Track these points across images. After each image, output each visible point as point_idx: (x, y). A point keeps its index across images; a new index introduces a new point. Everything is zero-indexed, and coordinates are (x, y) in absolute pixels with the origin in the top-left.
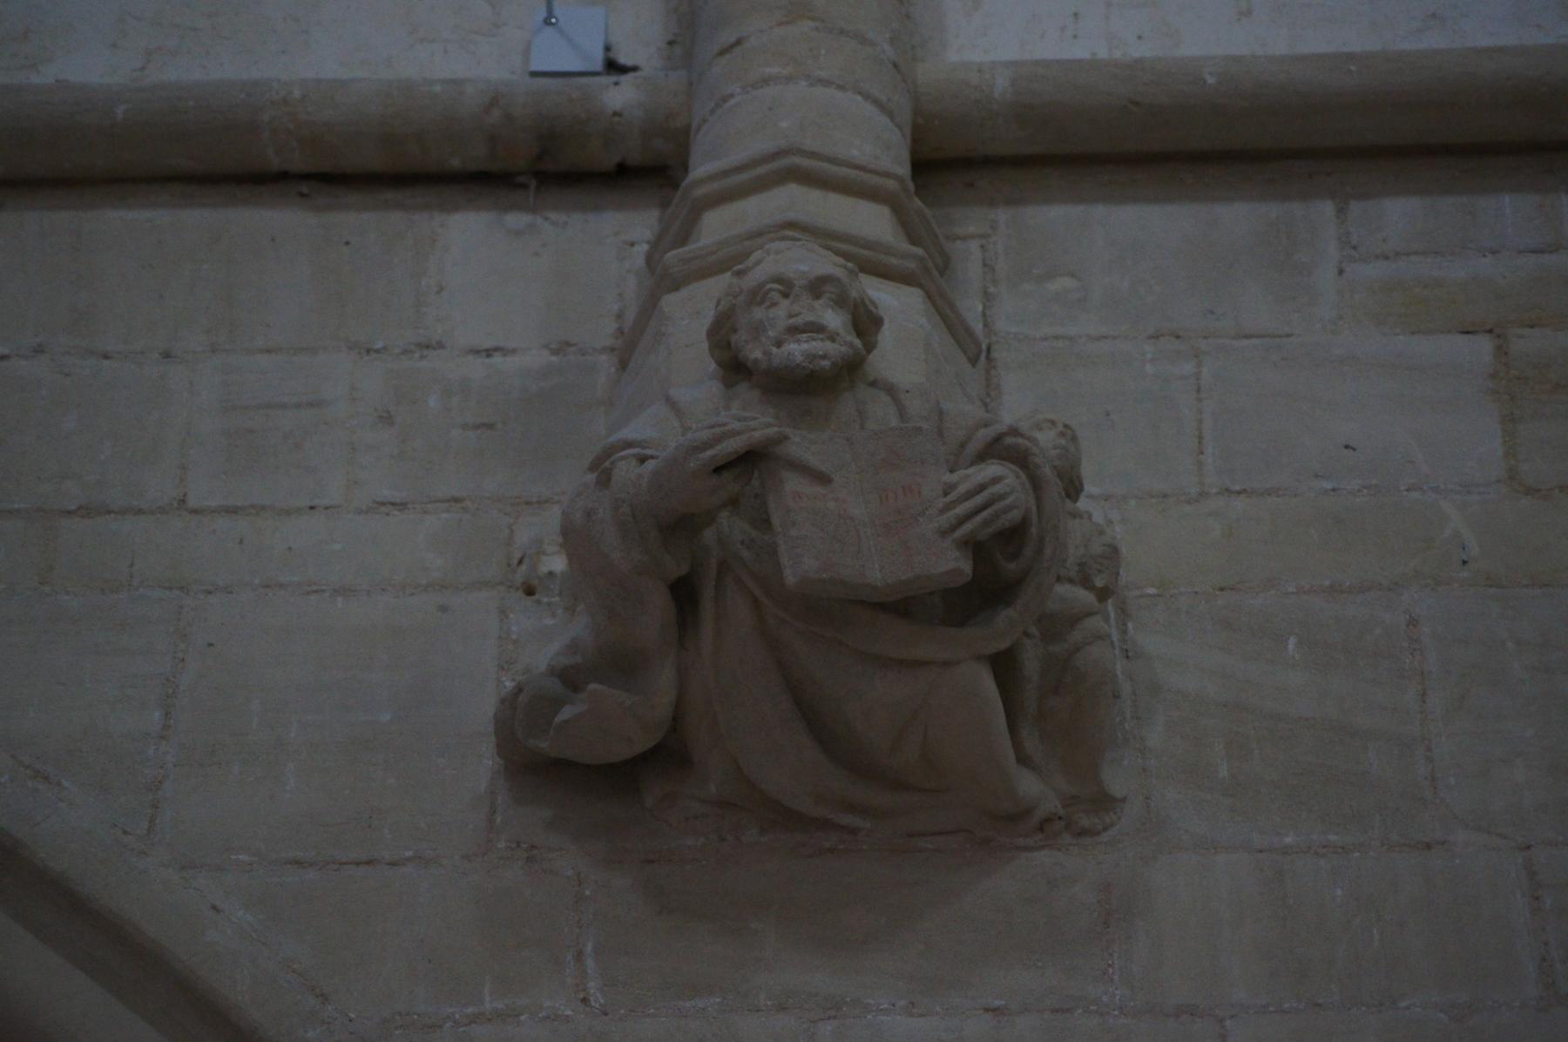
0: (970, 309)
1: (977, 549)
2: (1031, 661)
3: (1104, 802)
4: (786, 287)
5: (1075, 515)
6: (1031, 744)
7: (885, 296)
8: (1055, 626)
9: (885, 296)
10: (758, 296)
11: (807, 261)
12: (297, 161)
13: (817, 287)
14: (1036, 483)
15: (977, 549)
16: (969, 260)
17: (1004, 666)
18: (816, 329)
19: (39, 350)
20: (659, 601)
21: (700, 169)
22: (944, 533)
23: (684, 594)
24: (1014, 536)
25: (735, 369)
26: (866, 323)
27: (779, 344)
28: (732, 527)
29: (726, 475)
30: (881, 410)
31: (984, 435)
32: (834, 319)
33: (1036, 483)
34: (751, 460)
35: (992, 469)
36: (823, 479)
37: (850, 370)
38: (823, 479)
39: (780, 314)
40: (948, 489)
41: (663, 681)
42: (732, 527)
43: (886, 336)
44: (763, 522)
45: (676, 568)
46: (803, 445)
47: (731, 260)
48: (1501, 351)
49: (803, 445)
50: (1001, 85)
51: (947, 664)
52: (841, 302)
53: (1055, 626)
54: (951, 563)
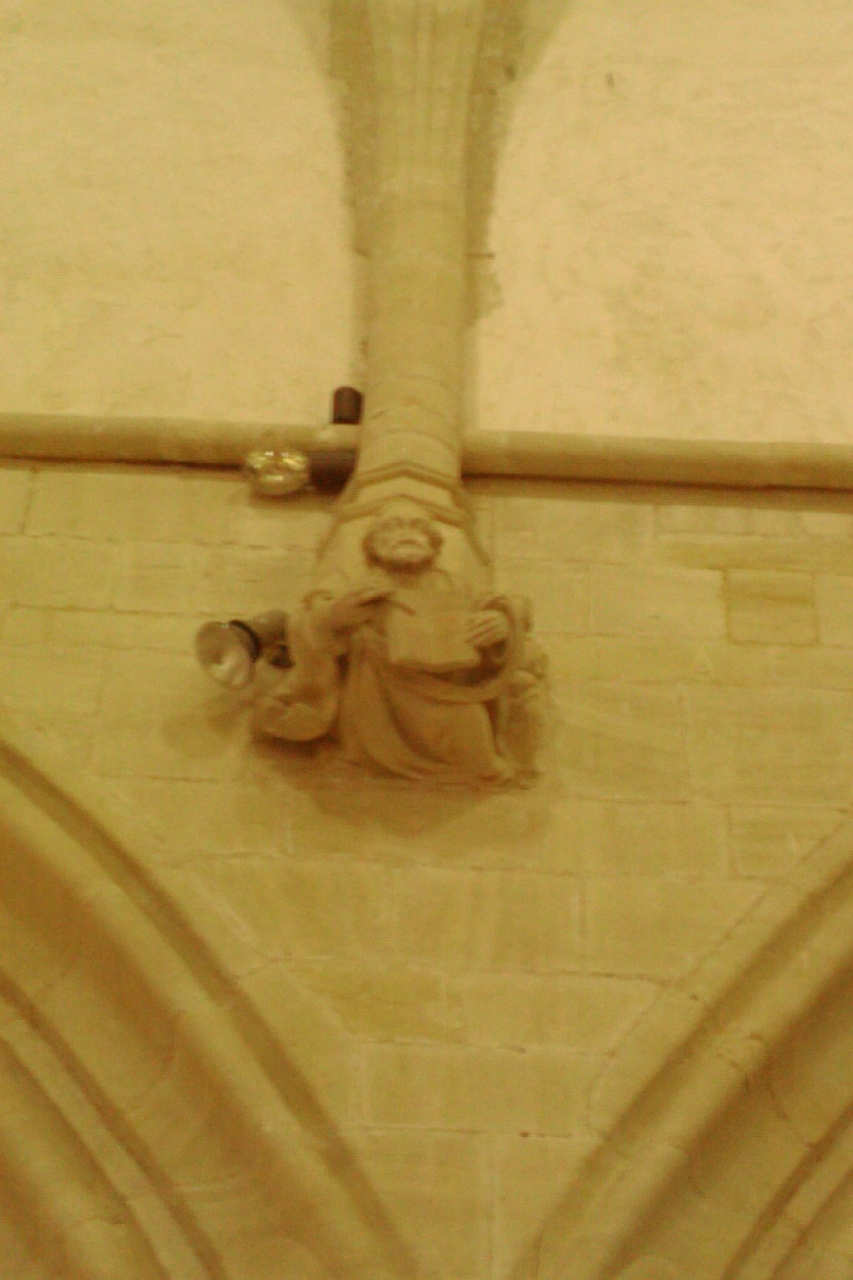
0: (484, 542)
1: (483, 651)
2: (504, 705)
3: (533, 774)
4: (399, 522)
5: (528, 639)
6: (502, 744)
7: (447, 532)
8: (515, 690)
9: (447, 532)
10: (386, 526)
11: (408, 511)
12: (175, 455)
13: (414, 523)
14: (512, 621)
15: (483, 651)
16: (484, 520)
17: (491, 707)
18: (411, 542)
19: (52, 534)
20: (330, 668)
21: (364, 467)
22: (468, 641)
23: (343, 663)
24: (500, 646)
25: (374, 560)
26: (436, 542)
27: (394, 548)
28: (368, 633)
29: (237, 628)
30: (441, 584)
31: (489, 598)
32: (422, 539)
33: (512, 621)
34: (379, 602)
35: (493, 614)
36: (410, 612)
37: (425, 565)
38: (410, 612)
39: (396, 535)
40: (471, 621)
41: (330, 706)
42: (368, 633)
43: (446, 549)
44: (382, 632)
45: (339, 650)
46: (404, 596)
47: (372, 511)
48: (725, 579)
49: (404, 596)
50: (503, 442)
51: (465, 704)
52: (426, 532)
53: (515, 690)
54: (468, 656)
